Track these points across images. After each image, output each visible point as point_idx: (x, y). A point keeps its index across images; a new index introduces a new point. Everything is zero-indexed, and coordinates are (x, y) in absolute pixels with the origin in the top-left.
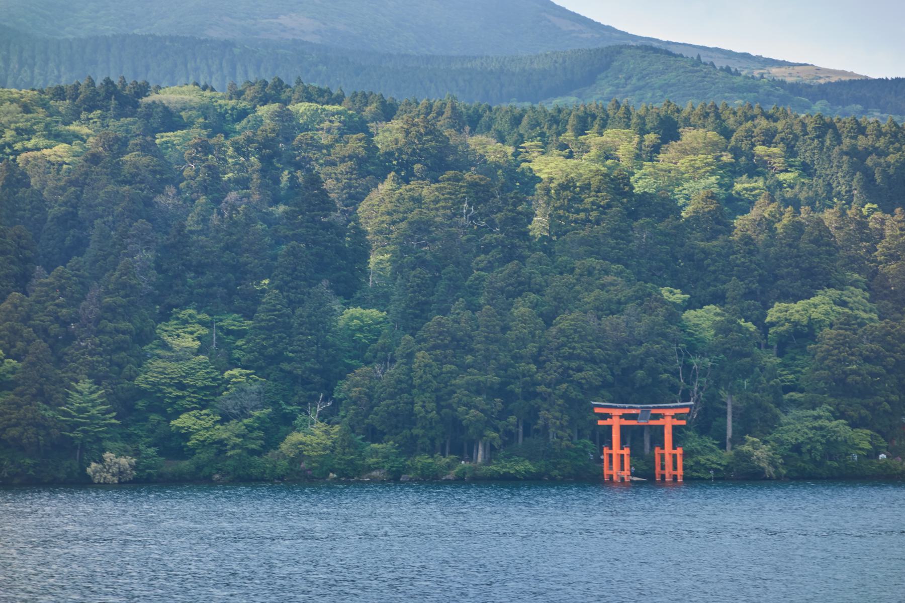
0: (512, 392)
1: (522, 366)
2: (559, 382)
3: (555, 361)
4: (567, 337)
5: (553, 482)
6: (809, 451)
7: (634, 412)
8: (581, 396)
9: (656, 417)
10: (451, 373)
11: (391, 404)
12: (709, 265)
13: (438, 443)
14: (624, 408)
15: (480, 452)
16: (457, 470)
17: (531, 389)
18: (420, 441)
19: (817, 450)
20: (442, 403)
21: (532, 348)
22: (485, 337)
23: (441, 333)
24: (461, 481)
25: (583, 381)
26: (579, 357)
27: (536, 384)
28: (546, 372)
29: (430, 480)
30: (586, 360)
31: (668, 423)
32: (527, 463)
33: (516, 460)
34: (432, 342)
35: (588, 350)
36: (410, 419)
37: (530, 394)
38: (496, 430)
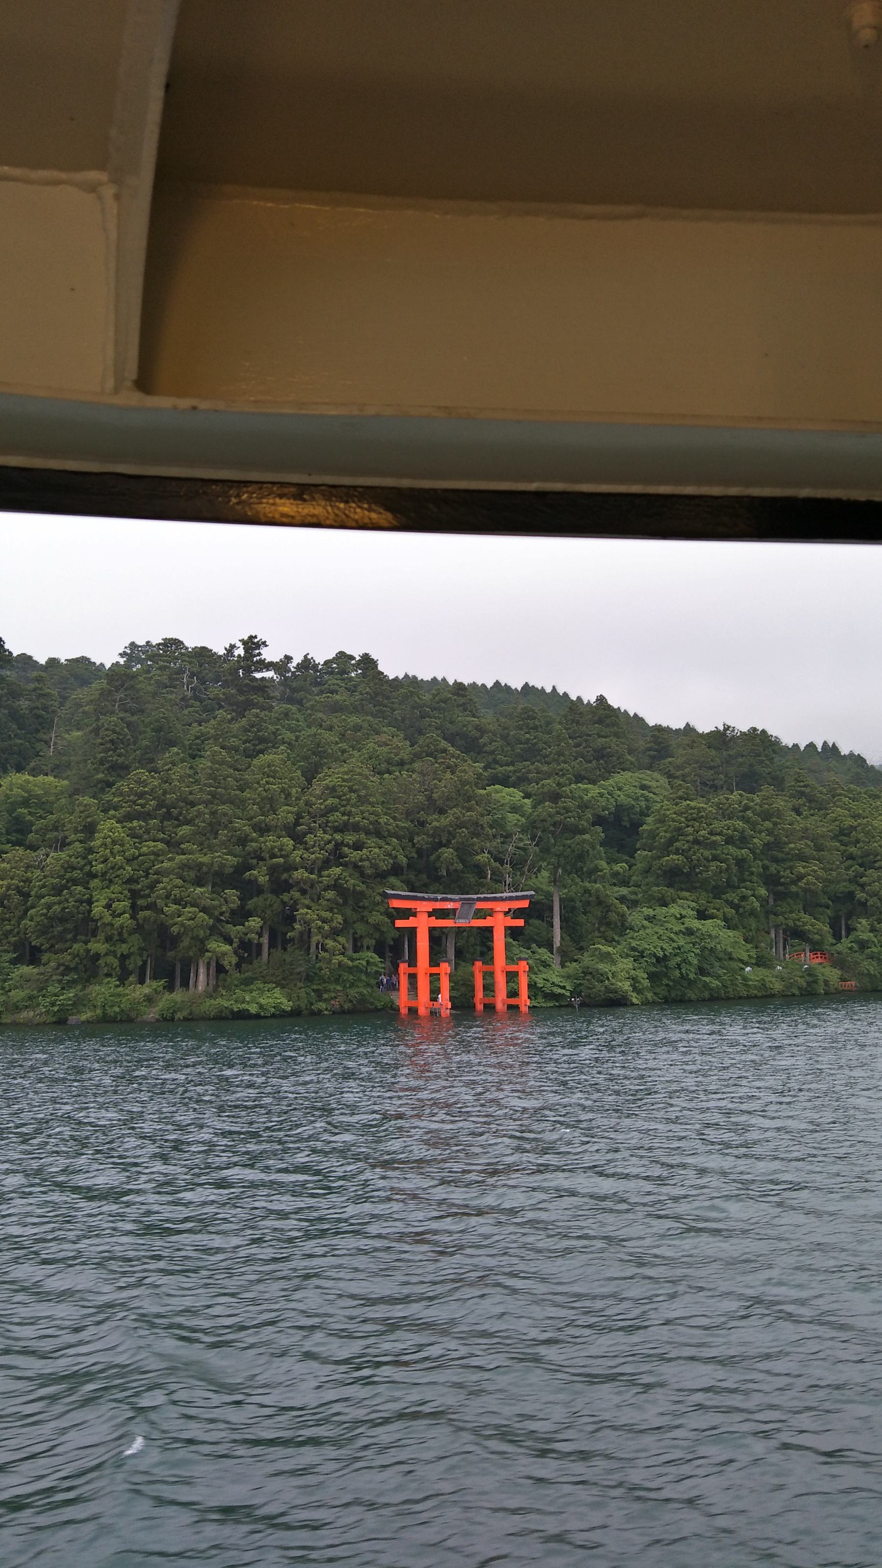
0: (253, 882)
1: (270, 841)
2: (326, 864)
3: (320, 833)
4: (339, 797)
5: (837, 997)
6: (679, 966)
7: (450, 906)
8: (362, 887)
9: (481, 914)
10: (157, 854)
11: (55, 903)
12: (485, 745)
13: (131, 965)
14: (436, 900)
15: (202, 977)
16: (161, 1005)
17: (285, 876)
18: (101, 962)
19: (690, 964)
20: (141, 902)
21: (285, 813)
22: (209, 793)
23: (141, 795)
24: (169, 1026)
25: (366, 863)
26: (356, 828)
27: (291, 868)
28: (307, 849)
29: (118, 1024)
30: (368, 833)
31: (499, 924)
32: (277, 992)
33: (259, 989)
34: (126, 809)
35: (372, 818)
36: (86, 926)
37: (280, 886)
38: (228, 940)
